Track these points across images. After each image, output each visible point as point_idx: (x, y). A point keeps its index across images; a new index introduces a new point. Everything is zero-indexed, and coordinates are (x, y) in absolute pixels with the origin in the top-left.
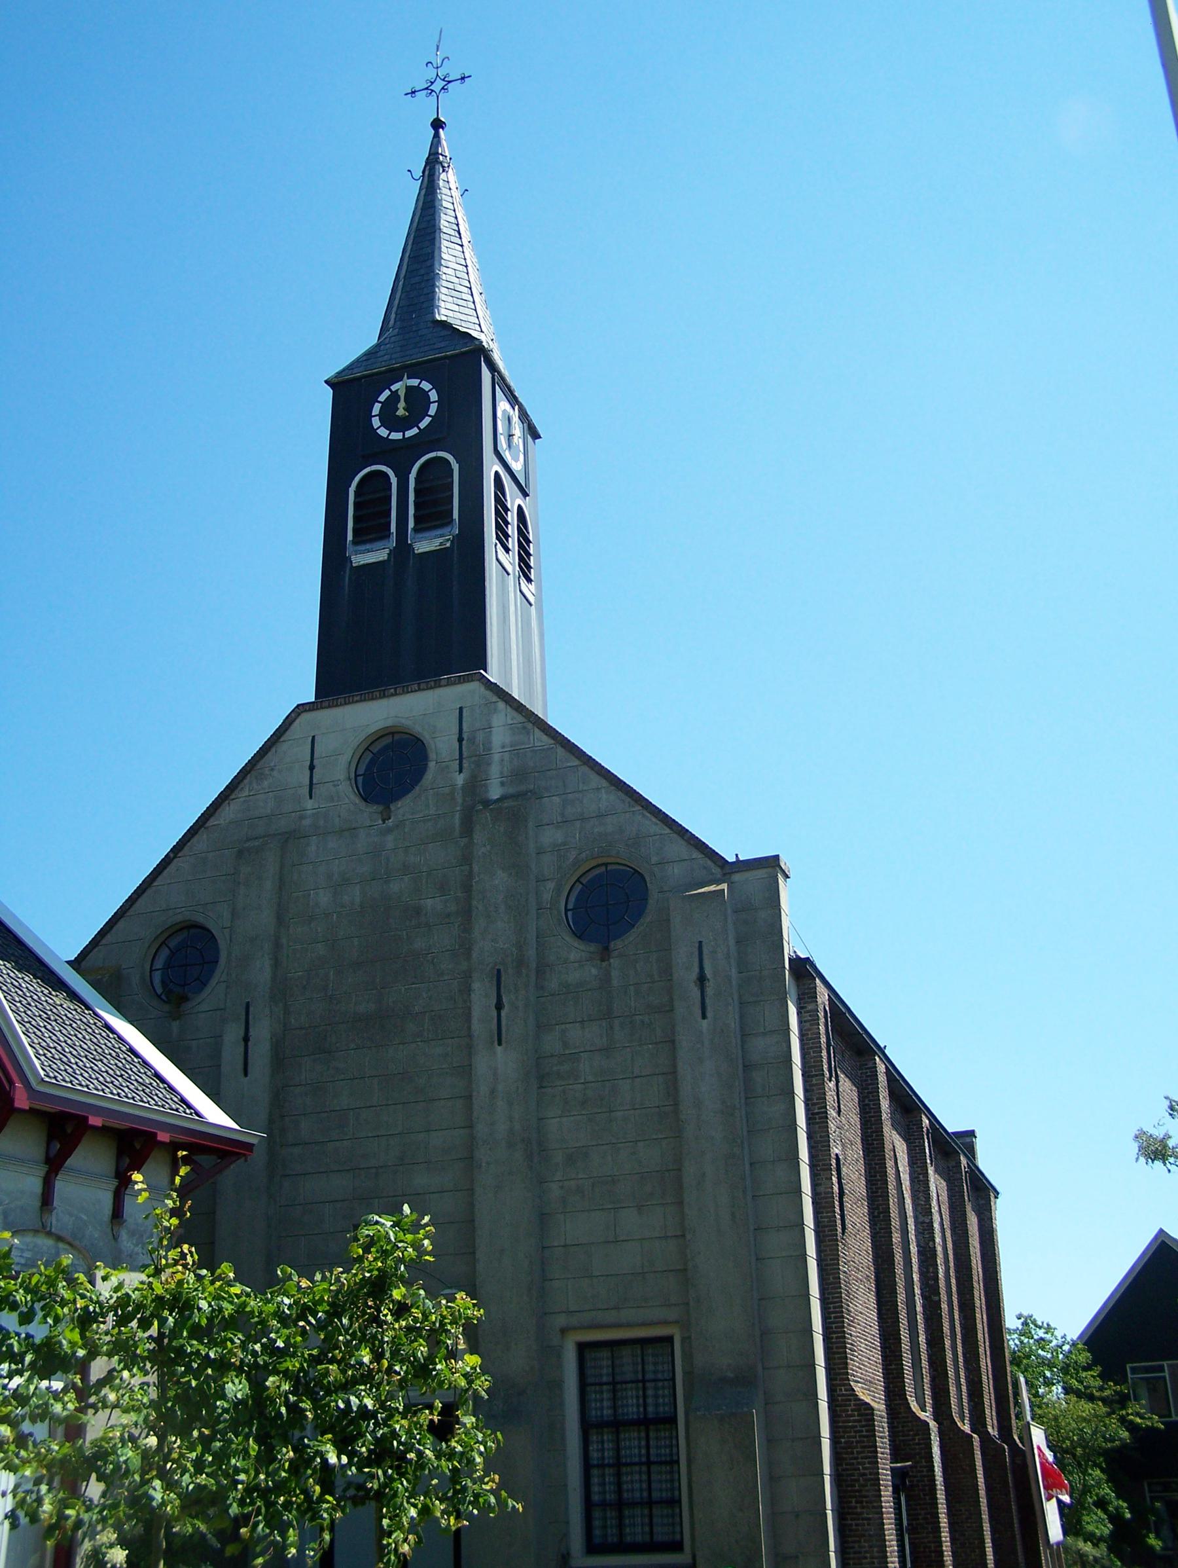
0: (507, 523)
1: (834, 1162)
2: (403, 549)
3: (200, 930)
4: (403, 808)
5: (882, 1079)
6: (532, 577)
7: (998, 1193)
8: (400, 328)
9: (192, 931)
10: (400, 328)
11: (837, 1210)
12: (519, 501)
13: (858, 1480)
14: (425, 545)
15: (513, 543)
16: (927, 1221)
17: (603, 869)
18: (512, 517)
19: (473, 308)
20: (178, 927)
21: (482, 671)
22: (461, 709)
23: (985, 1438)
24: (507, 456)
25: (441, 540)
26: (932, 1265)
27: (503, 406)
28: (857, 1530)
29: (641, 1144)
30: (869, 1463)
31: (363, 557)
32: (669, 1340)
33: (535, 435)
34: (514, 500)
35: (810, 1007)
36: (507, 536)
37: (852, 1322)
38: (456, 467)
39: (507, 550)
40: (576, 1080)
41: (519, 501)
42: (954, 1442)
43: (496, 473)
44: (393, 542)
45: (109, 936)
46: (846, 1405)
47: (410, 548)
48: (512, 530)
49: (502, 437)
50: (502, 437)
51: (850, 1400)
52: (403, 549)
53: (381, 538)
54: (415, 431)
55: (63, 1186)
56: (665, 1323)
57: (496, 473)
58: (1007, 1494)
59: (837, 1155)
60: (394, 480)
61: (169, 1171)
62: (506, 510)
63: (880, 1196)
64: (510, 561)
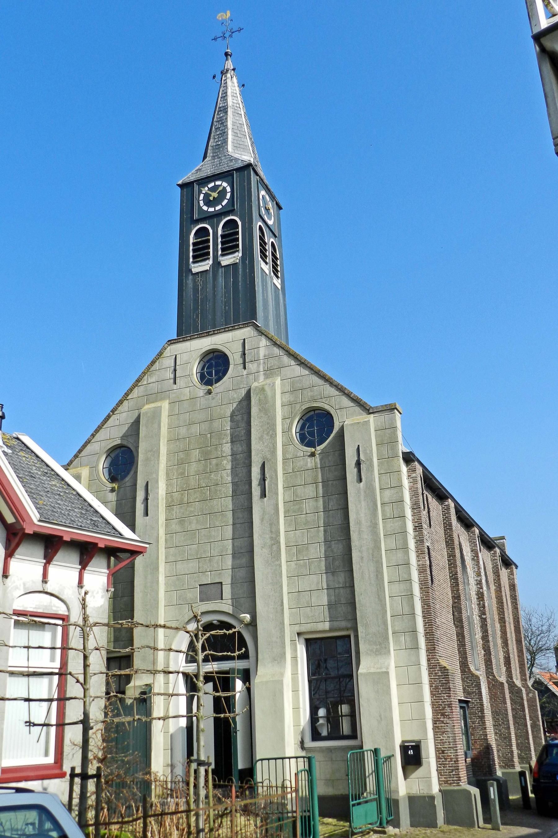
0: (266, 250)
1: (426, 550)
2: (217, 264)
3: (126, 448)
4: (218, 387)
5: (453, 511)
6: (279, 275)
7: (517, 566)
8: (212, 157)
9: (122, 449)
10: (212, 157)
11: (429, 572)
12: (272, 240)
13: (441, 705)
14: (226, 261)
15: (269, 259)
16: (479, 579)
17: (312, 413)
18: (269, 247)
19: (41, 727)
20: (115, 447)
21: (254, 321)
22: (244, 340)
23: (512, 685)
24: (266, 218)
25: (234, 259)
26: (482, 601)
27: (263, 193)
28: (442, 729)
29: (333, 542)
30: (447, 696)
31: (197, 268)
32: (349, 637)
33: (280, 208)
34: (269, 240)
35: (414, 475)
36: (266, 256)
37: (437, 627)
38: (240, 223)
39: (266, 263)
40: (301, 512)
41: (272, 240)
42: (495, 685)
43: (260, 226)
44: (210, 262)
45: (83, 453)
46: (435, 668)
47: (219, 263)
48: (269, 253)
49: (262, 208)
50: (262, 208)
51: (436, 666)
52: (217, 264)
53: (205, 260)
54: (220, 207)
55: (87, 576)
56: (347, 629)
57: (260, 226)
58: (524, 710)
59: (428, 546)
60: (211, 231)
61: (106, 562)
62: (265, 244)
63: (452, 567)
64: (267, 268)
